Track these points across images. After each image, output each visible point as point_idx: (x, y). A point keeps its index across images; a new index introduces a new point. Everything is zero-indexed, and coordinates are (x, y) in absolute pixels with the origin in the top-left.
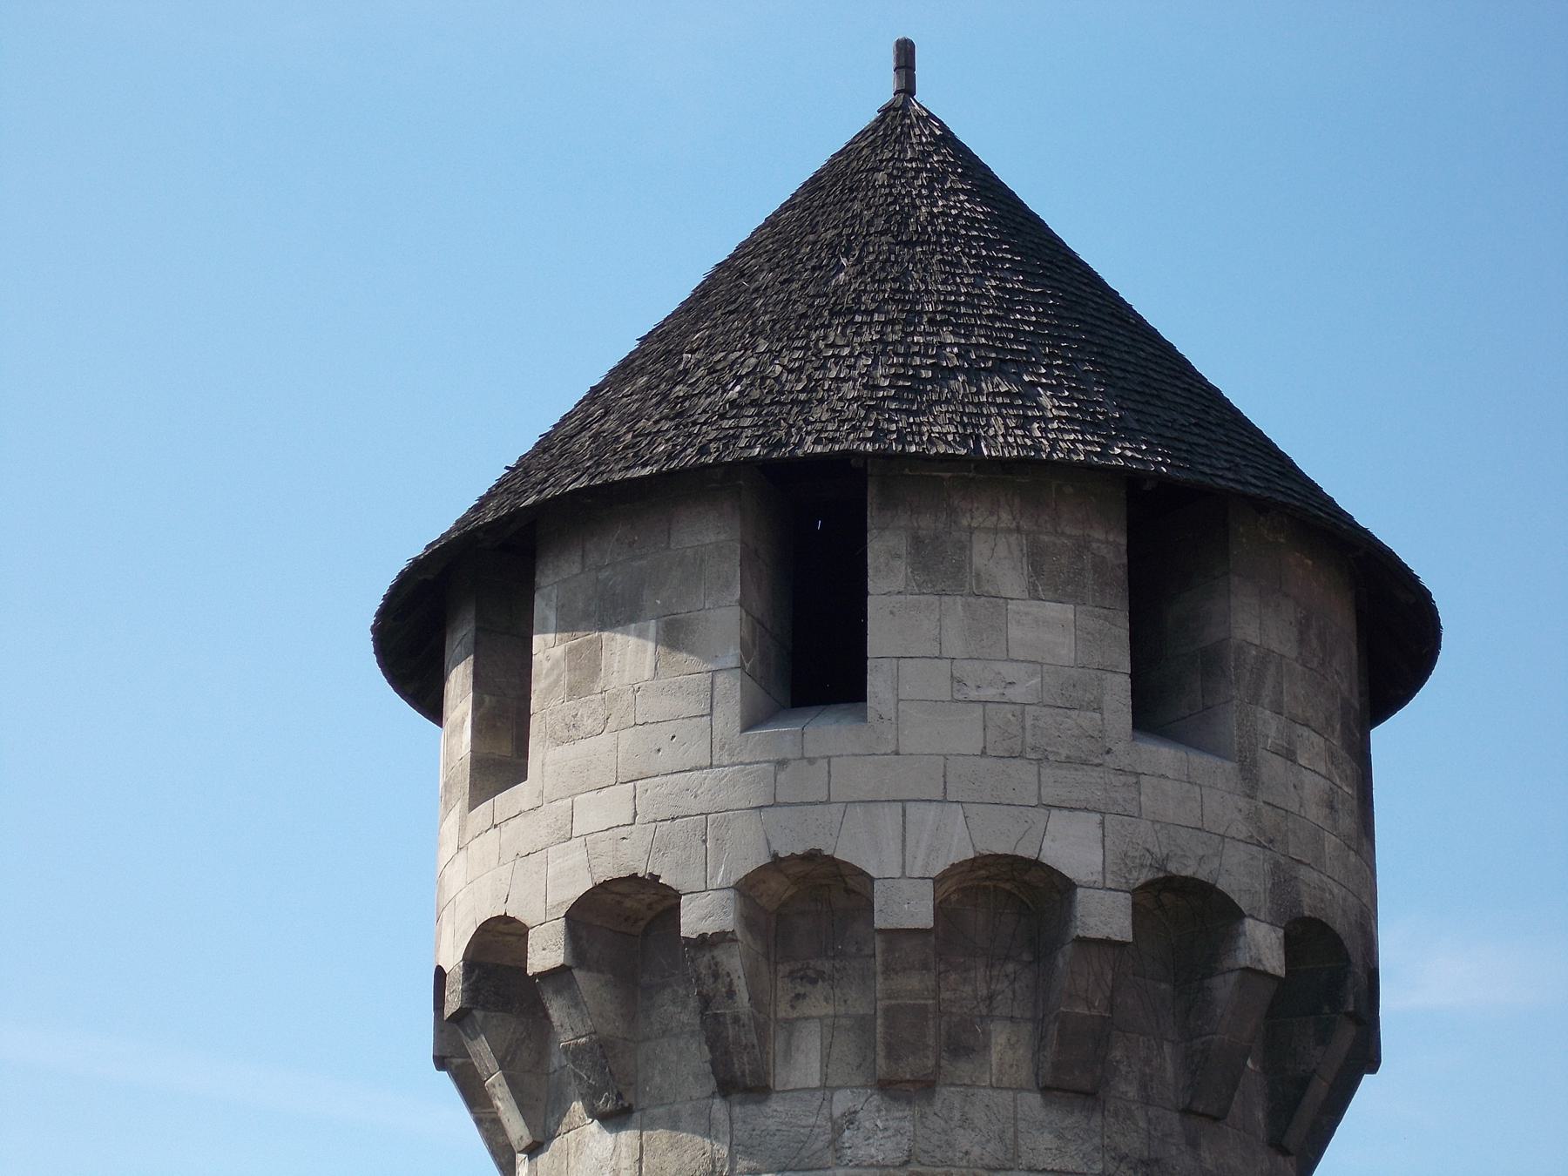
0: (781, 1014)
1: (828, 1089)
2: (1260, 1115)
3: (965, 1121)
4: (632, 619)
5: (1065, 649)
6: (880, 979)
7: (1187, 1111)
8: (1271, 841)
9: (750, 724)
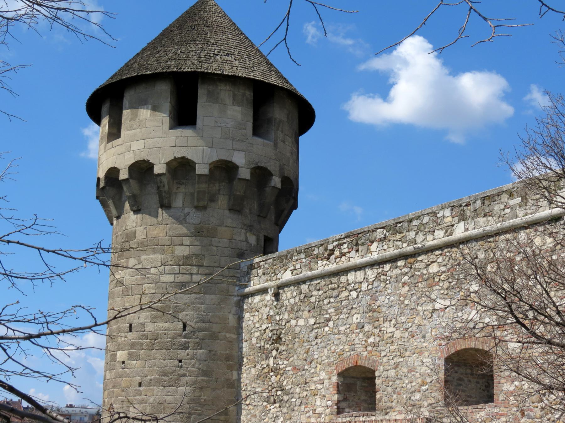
0: (174, 191)
2: (273, 217)
4: (146, 104)
5: (239, 117)
6: (196, 185)
7: (259, 216)
8: (280, 160)
9: (171, 128)
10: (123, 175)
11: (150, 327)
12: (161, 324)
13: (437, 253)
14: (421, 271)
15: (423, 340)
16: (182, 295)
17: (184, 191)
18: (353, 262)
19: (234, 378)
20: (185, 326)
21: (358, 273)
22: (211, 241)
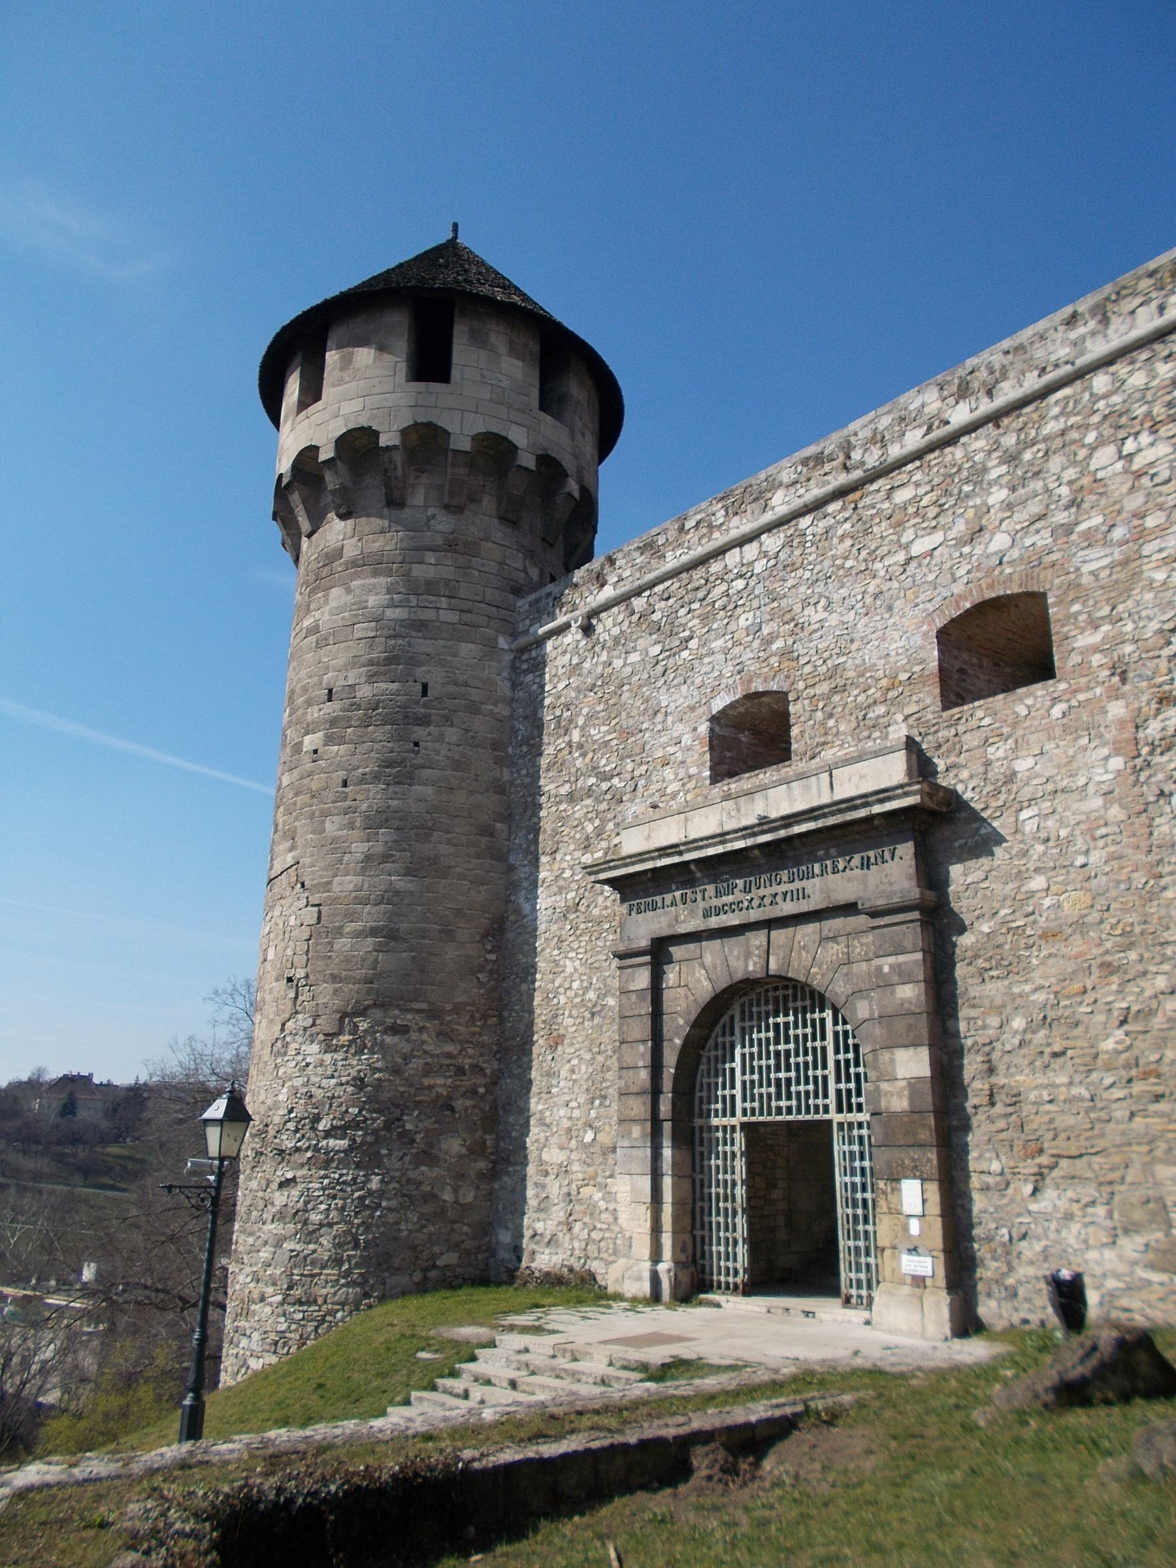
1: (426, 506)
3: (473, 523)
5: (519, 375)
9: (408, 381)
10: (326, 454)
11: (365, 692)
12: (383, 686)
13: (910, 467)
14: (878, 506)
15: (886, 616)
16: (421, 641)
17: (428, 482)
18: (734, 533)
19: (505, 779)
20: (425, 688)
21: (746, 548)
22: (470, 561)
